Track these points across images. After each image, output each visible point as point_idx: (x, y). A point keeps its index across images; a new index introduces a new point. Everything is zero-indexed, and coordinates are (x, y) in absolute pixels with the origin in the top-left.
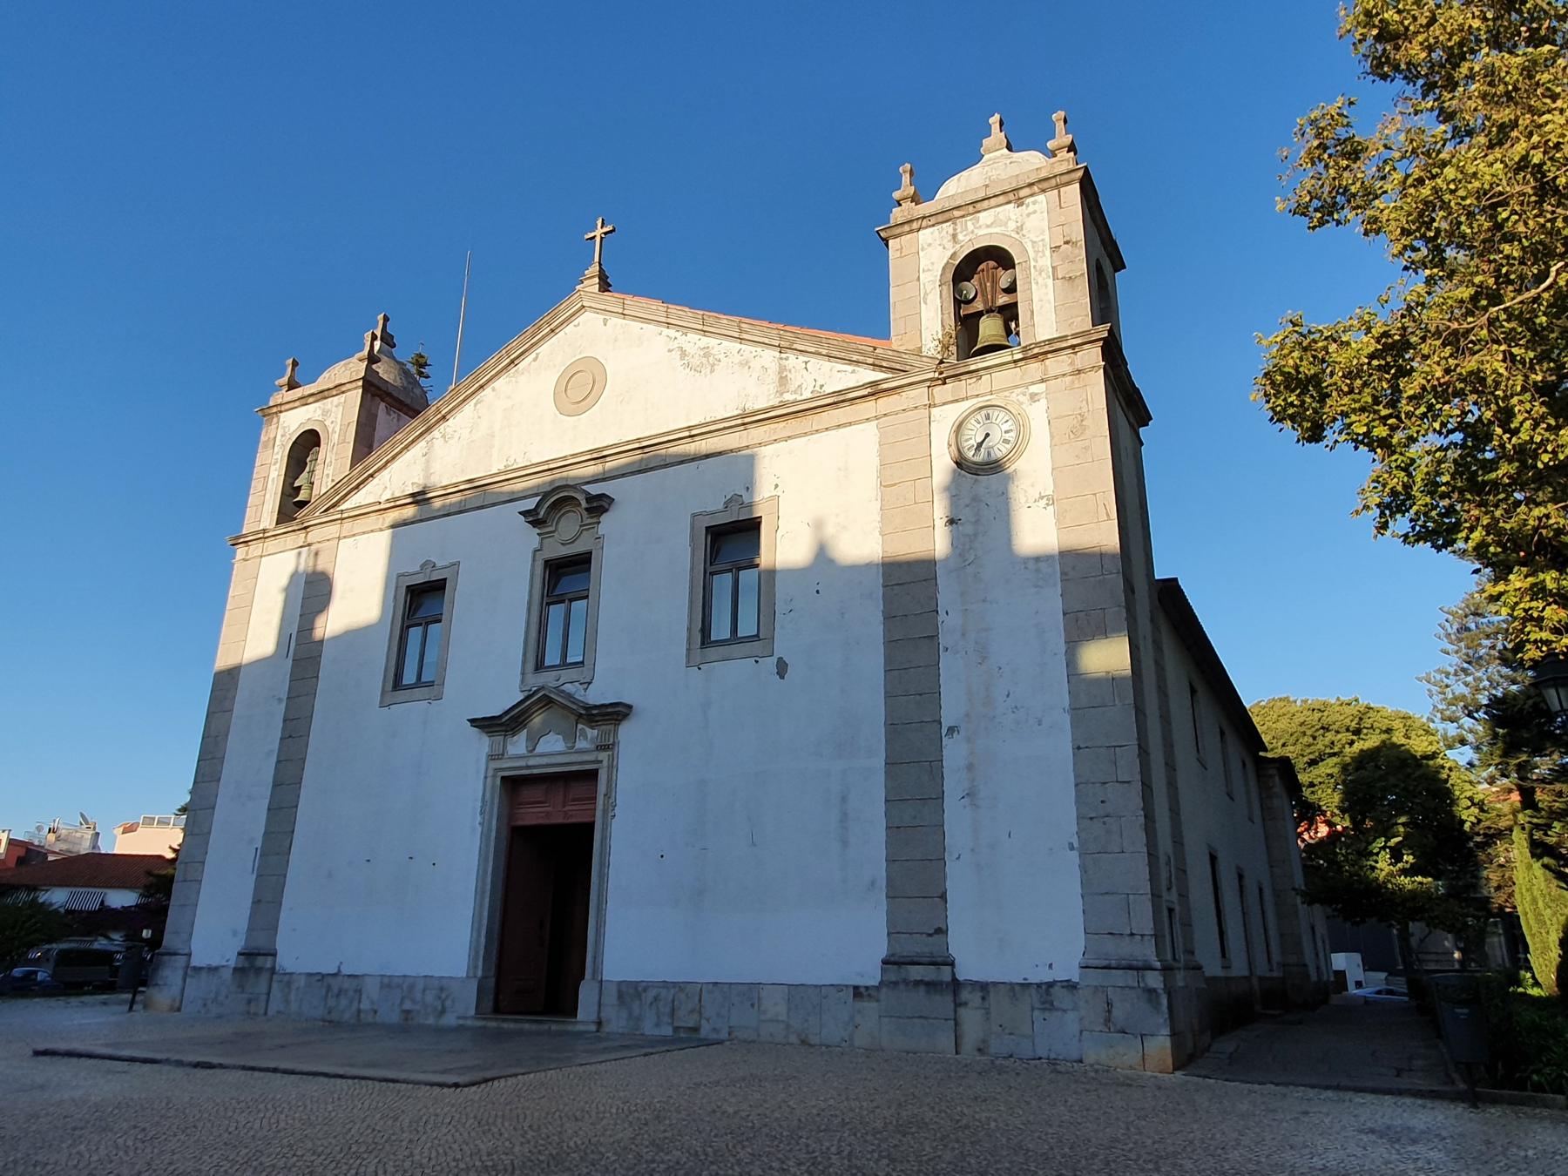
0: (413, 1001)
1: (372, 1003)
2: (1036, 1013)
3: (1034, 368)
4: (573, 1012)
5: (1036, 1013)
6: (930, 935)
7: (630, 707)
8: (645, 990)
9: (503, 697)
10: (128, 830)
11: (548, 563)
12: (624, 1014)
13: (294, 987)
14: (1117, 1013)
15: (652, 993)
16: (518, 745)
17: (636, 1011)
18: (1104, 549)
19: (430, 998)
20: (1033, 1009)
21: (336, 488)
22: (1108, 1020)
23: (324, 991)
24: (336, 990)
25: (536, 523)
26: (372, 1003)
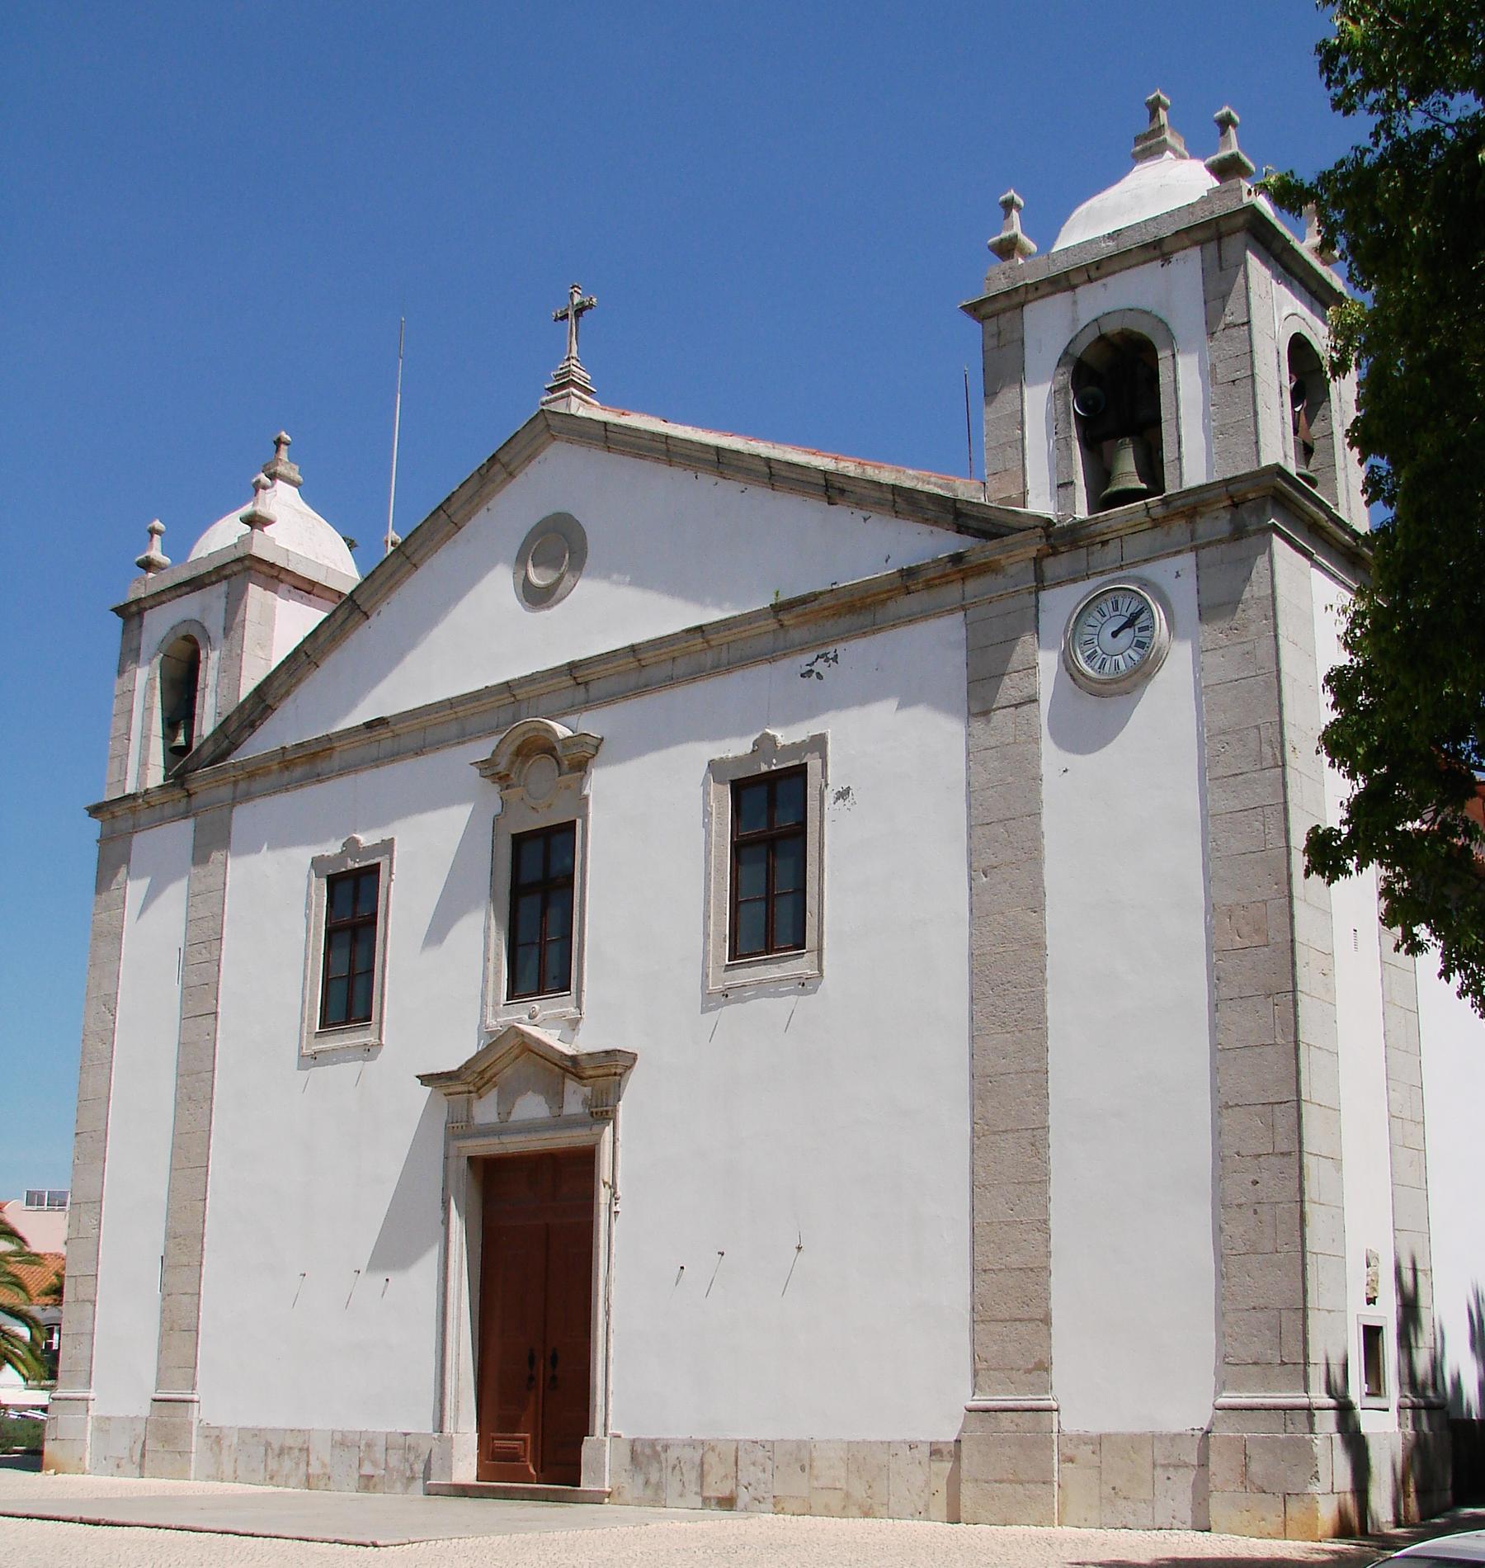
0: (375, 1464)
1: (324, 1465)
2: (1159, 1471)
3: (1179, 529)
4: (1233, 156)
5: (1159, 1471)
6: (1029, 1371)
7: (634, 1057)
8: (666, 1448)
9: (456, 1049)
10: (34, 1199)
11: (519, 841)
12: (640, 1479)
13: (225, 1443)
14: (1255, 1467)
15: (672, 1454)
16: (486, 1111)
17: (654, 1477)
18: (800, 498)
19: (394, 1461)
20: (1154, 1466)
21: (221, 729)
22: (1245, 1474)
23: (262, 1449)
24: (276, 1446)
25: (502, 779)
26: (324, 1465)
